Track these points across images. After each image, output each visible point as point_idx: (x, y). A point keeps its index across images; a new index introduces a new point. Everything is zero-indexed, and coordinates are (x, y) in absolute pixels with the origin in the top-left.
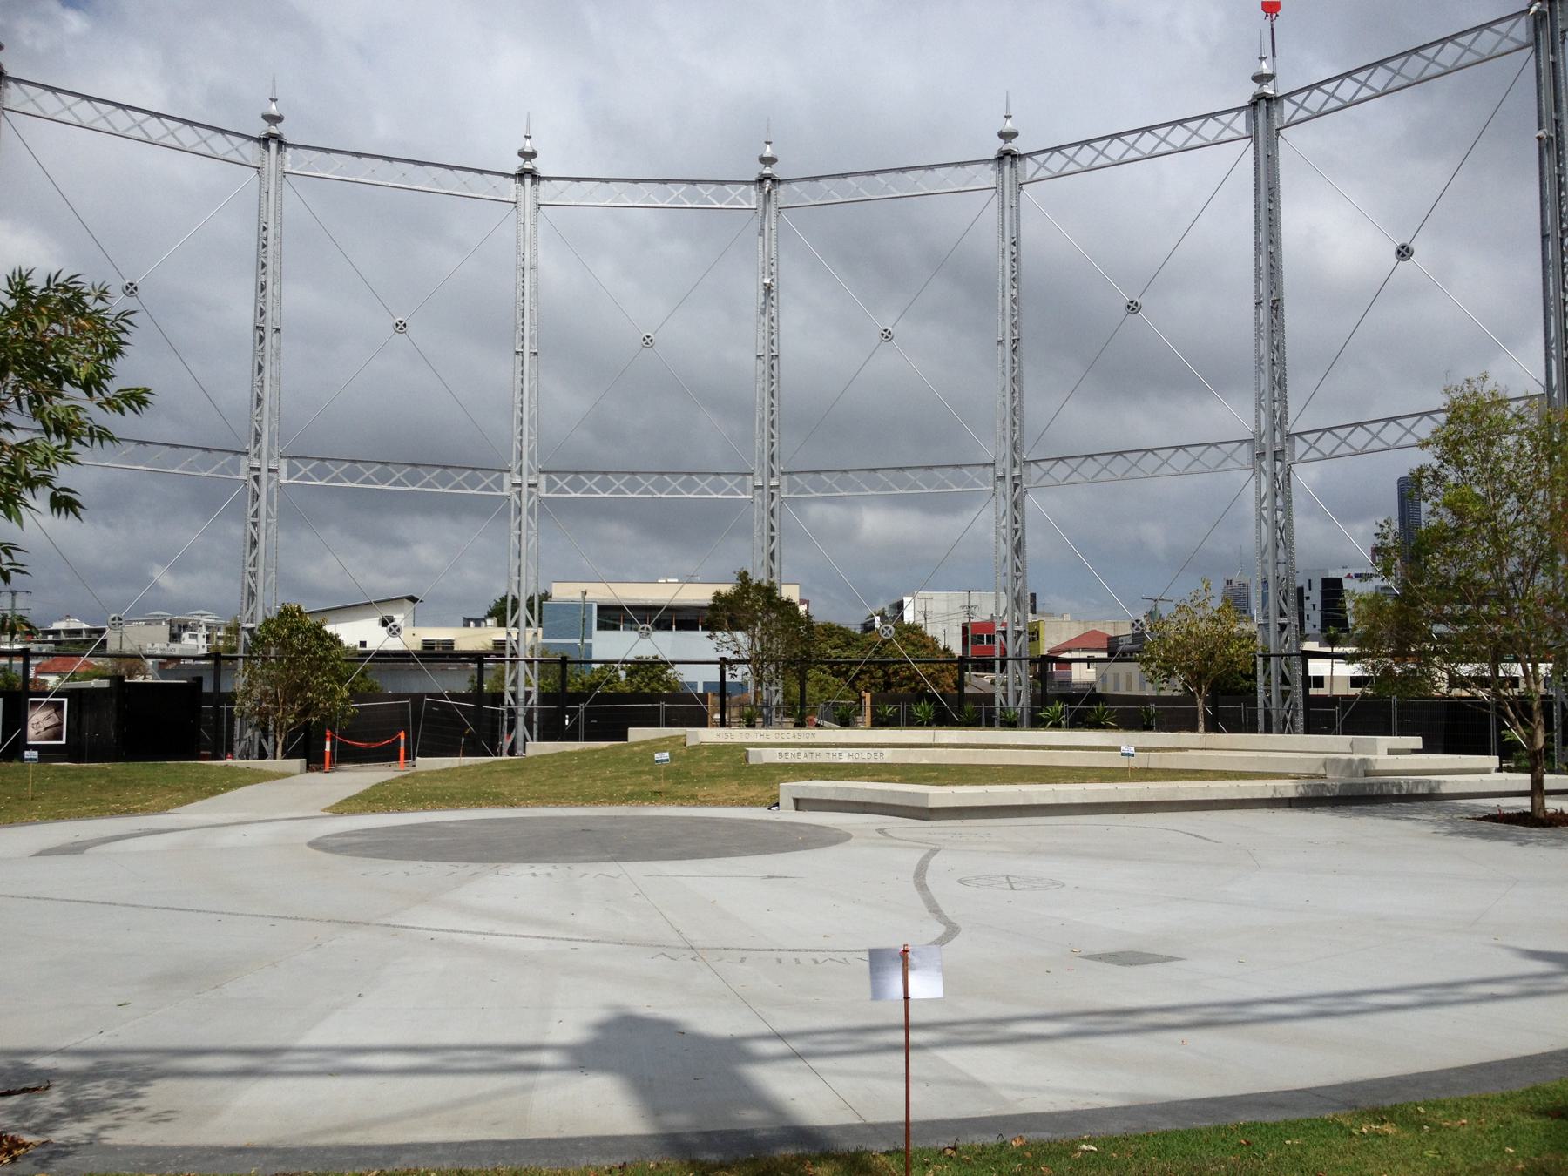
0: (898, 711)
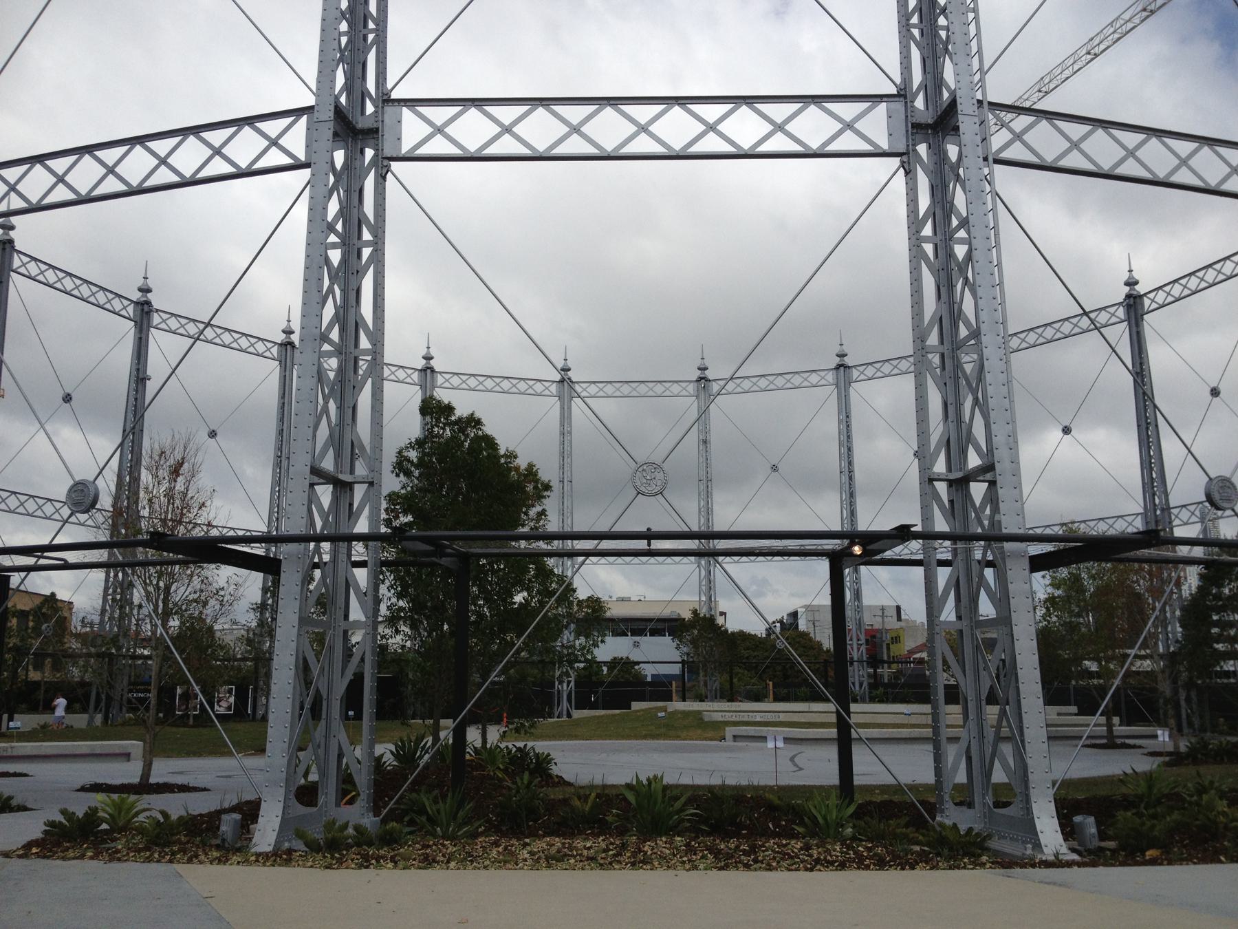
0: (789, 692)
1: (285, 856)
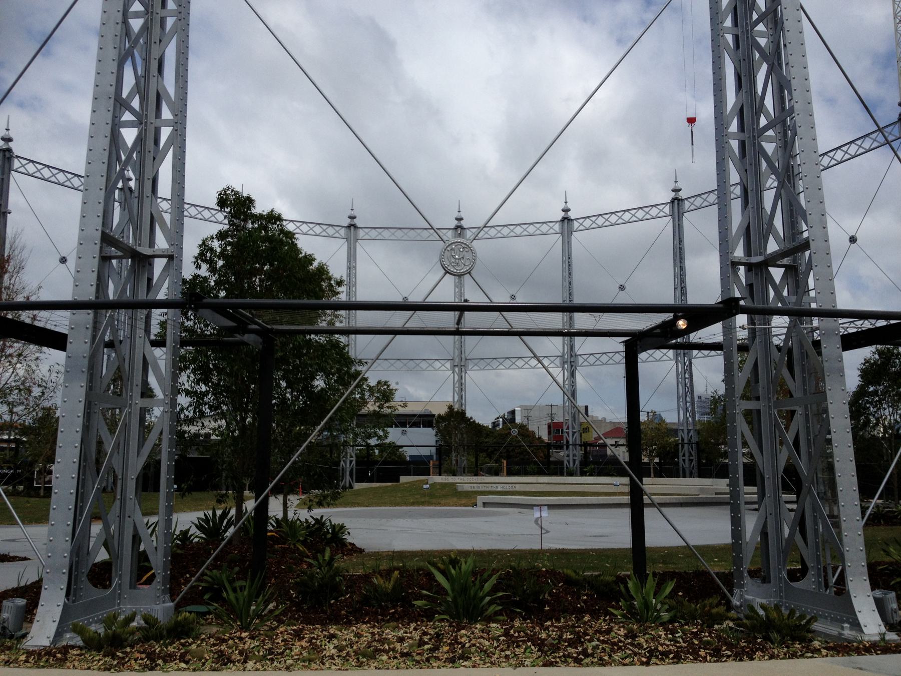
1: (59, 655)
